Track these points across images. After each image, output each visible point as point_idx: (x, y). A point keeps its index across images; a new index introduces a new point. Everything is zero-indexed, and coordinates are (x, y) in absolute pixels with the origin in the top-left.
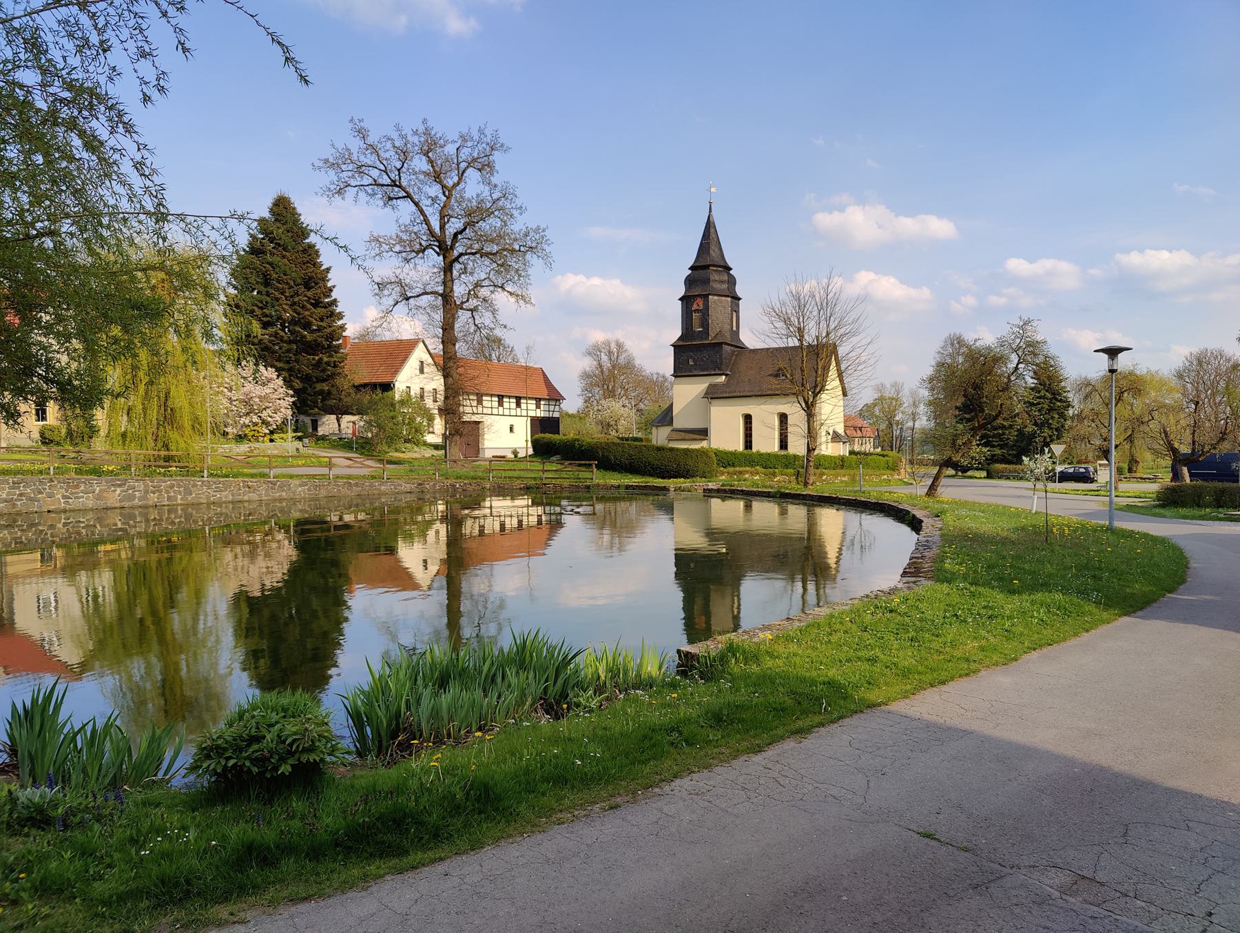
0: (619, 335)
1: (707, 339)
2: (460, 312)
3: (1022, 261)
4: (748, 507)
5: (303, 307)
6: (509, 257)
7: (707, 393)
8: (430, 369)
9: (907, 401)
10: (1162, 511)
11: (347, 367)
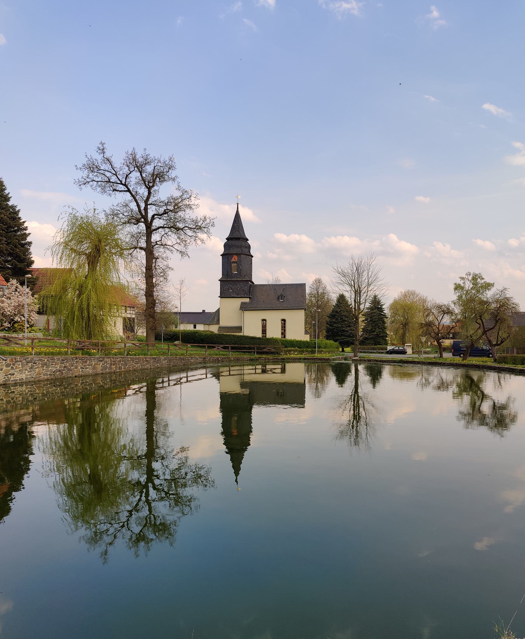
5: (16, 246)
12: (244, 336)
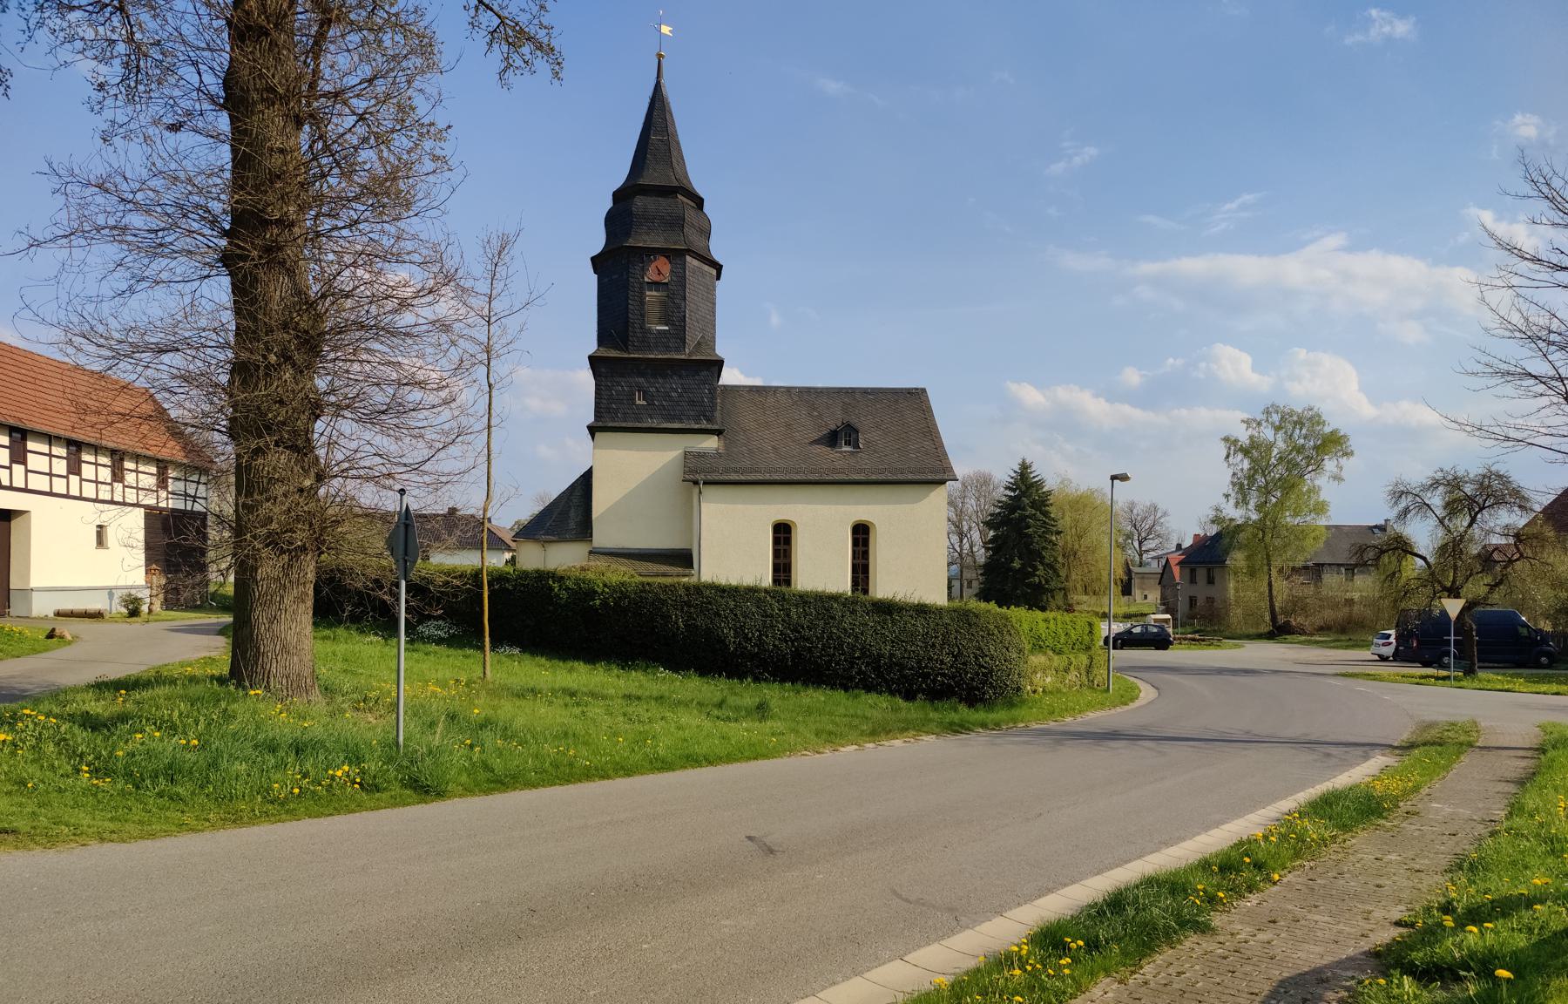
12: (699, 589)
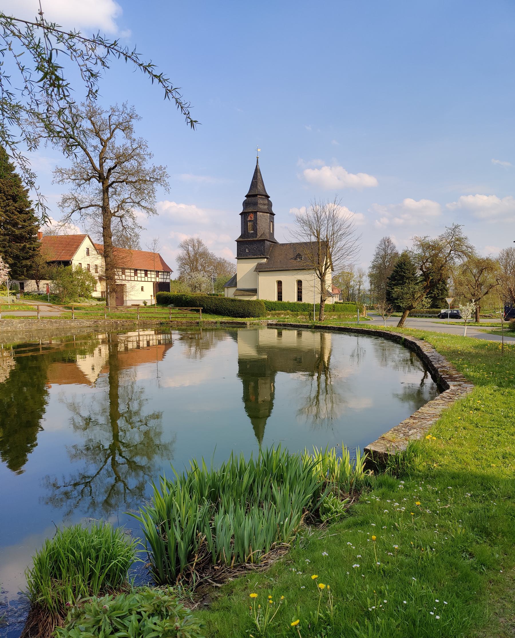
0: (195, 237)
1: (256, 237)
2: (113, 218)
3: (412, 200)
4: (299, 335)
5: (13, 213)
6: (143, 184)
7: (256, 269)
8: (93, 252)
9: (356, 275)
10: (512, 334)
11: (42, 251)
